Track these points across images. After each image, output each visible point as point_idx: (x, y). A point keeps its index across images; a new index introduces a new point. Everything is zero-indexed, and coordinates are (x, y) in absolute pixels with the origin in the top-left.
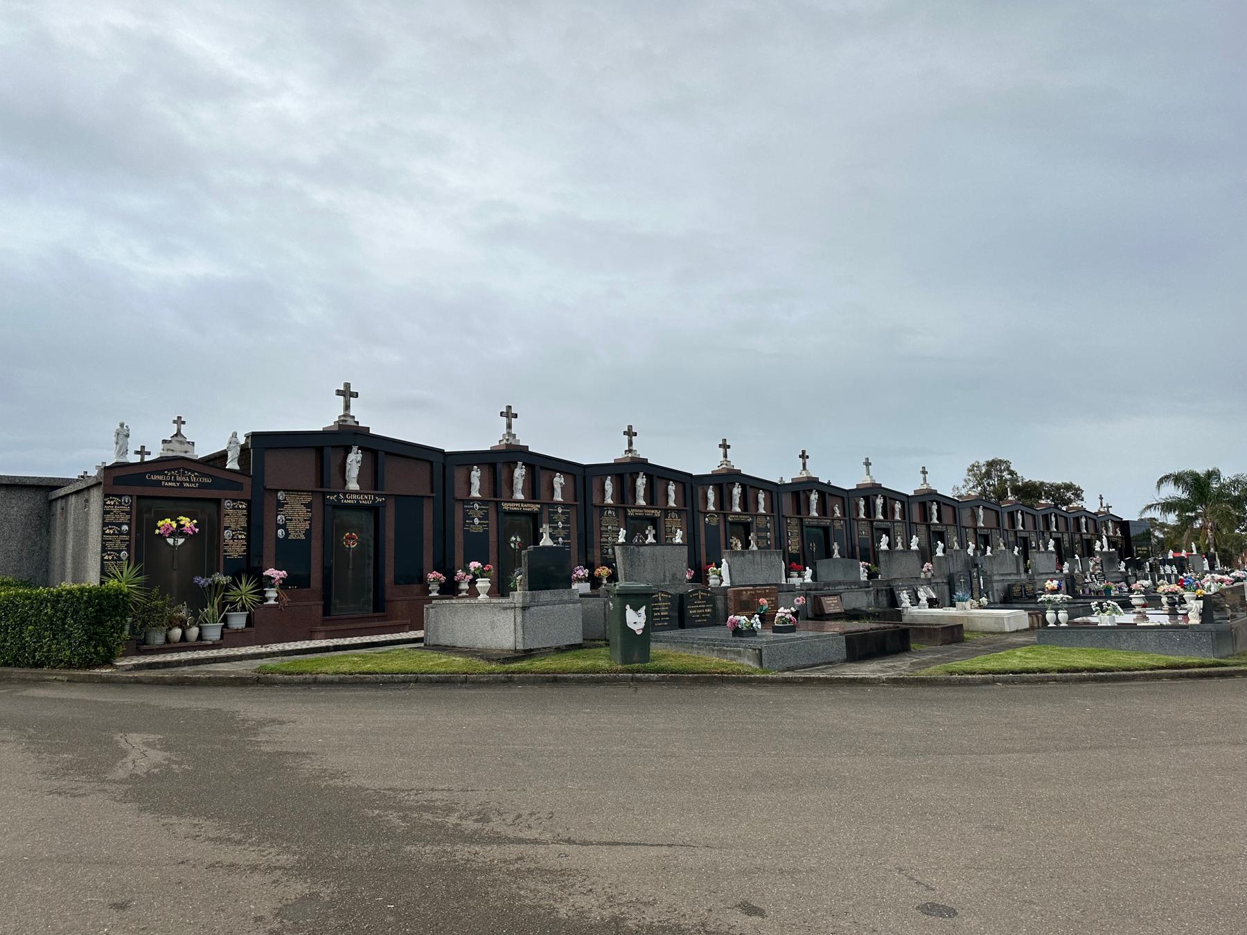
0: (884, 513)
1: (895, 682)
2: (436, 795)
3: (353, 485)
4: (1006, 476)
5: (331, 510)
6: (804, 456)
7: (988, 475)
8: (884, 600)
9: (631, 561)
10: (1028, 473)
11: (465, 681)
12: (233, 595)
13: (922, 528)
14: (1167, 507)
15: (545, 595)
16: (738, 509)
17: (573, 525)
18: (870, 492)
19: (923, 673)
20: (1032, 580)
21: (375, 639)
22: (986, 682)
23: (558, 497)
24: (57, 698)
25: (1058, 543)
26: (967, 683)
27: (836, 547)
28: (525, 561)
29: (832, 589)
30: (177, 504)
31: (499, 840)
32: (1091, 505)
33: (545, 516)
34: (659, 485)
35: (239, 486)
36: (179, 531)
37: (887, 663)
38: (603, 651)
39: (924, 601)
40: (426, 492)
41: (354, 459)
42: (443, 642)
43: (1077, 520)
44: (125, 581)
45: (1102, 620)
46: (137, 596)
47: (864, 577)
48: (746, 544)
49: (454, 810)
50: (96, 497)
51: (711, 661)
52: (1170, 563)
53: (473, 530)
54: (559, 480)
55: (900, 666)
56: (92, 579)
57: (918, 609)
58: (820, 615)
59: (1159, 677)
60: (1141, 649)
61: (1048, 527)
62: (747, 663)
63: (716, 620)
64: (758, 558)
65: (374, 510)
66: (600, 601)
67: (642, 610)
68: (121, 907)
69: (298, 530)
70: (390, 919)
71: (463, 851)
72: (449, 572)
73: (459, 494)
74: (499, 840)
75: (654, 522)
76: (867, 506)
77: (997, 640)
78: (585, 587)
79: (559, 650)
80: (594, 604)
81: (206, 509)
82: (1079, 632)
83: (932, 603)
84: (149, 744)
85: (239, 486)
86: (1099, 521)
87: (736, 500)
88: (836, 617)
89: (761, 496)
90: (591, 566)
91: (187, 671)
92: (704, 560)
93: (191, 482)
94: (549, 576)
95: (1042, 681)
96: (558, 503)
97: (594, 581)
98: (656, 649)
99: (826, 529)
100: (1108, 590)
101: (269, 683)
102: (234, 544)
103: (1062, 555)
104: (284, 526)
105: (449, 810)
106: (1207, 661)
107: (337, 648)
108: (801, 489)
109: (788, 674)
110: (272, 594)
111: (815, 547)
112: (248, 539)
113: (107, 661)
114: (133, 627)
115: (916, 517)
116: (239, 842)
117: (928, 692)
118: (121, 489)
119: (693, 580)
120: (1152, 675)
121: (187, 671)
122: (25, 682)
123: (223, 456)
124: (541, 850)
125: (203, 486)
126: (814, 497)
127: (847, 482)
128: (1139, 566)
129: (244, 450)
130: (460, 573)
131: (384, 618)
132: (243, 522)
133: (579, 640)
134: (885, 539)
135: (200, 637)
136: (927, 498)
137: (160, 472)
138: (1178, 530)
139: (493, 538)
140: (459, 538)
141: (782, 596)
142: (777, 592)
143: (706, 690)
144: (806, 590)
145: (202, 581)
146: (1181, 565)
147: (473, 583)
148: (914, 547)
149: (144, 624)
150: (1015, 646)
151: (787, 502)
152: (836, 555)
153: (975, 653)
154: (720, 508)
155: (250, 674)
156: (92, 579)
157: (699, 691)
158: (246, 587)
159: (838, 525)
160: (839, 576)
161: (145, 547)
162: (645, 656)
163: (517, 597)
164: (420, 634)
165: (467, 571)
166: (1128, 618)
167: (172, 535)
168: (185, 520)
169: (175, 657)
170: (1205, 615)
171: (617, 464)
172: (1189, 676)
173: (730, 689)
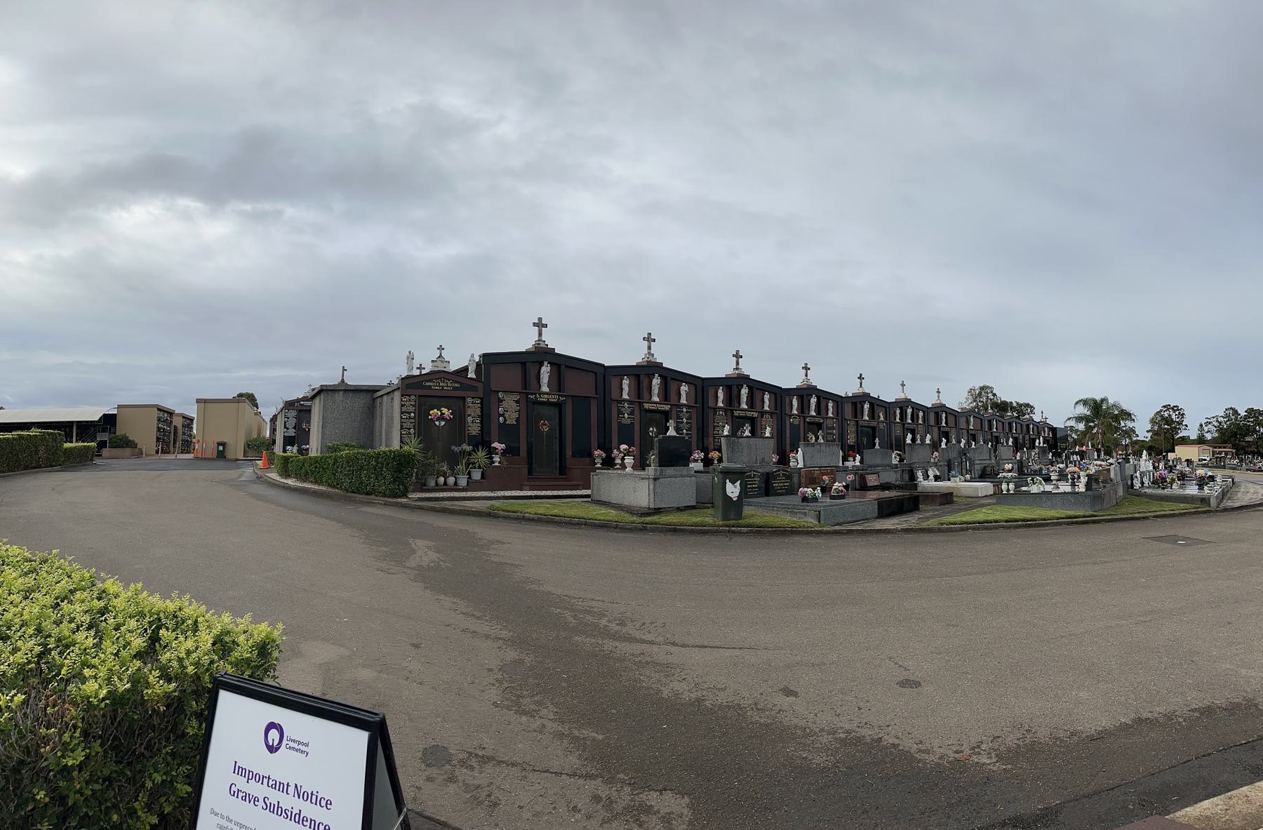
0: (912, 419)
1: (906, 531)
2: (594, 604)
3: (545, 389)
4: (990, 396)
5: (531, 405)
6: (861, 378)
7: (980, 394)
8: (906, 477)
9: (732, 447)
10: (1004, 395)
11: (616, 527)
12: (473, 458)
13: (936, 429)
14: (1079, 419)
15: (670, 471)
16: (813, 413)
17: (694, 421)
18: (903, 404)
19: (924, 525)
20: (998, 464)
21: (560, 493)
22: (962, 529)
23: (683, 401)
24: (379, 513)
25: (1016, 440)
26: (950, 530)
27: (877, 441)
28: (656, 445)
29: (873, 469)
30: (442, 399)
31: (630, 639)
32: (1037, 418)
33: (674, 414)
34: (757, 394)
35: (476, 389)
36: (442, 418)
37: (903, 518)
38: (710, 511)
39: (931, 477)
40: (592, 394)
41: (546, 370)
42: (604, 498)
43: (1028, 426)
44: (412, 447)
45: (1034, 489)
46: (419, 456)
47: (895, 461)
48: (817, 438)
49: (605, 616)
50: (397, 395)
51: (786, 519)
52: (1077, 453)
53: (624, 421)
54: (684, 388)
55: (911, 520)
56: (396, 445)
57: (927, 483)
58: (864, 487)
59: (1060, 524)
60: (1053, 507)
61: (1011, 430)
62: (810, 521)
63: (791, 491)
64: (823, 448)
65: (559, 406)
66: (709, 476)
67: (738, 484)
68: (416, 646)
69: (511, 418)
70: (564, 684)
71: (609, 645)
72: (609, 451)
73: (615, 396)
74: (630, 639)
75: (752, 421)
76: (901, 414)
77: (974, 502)
78: (699, 466)
79: (679, 509)
80: (705, 478)
81: (456, 403)
82: (1020, 497)
83: (937, 478)
84: (429, 548)
85: (476, 389)
86: (1040, 427)
87: (813, 407)
88: (875, 488)
89: (830, 405)
90: (706, 451)
91: (447, 504)
92: (788, 449)
93: (448, 385)
94: (674, 456)
95: (996, 528)
96: (684, 405)
97: (707, 462)
98: (747, 510)
99: (874, 429)
100: (1041, 470)
101: (496, 517)
102: (474, 428)
103: (1017, 447)
104: (503, 415)
105: (602, 615)
106: (1087, 513)
107: (537, 497)
108: (857, 401)
109: (837, 528)
110: (497, 459)
111: (865, 441)
112: (482, 423)
113: (404, 495)
114: (417, 477)
115: (932, 422)
116: (479, 618)
117: (926, 537)
118: (409, 391)
119: (778, 463)
120: (1057, 523)
121: (447, 504)
122: (362, 503)
123: (466, 369)
124: (656, 648)
125: (455, 389)
126: (867, 406)
127: (889, 397)
128: (1060, 455)
129: (478, 365)
130: (615, 451)
131: (566, 480)
132: (478, 412)
133: (693, 503)
134: (909, 436)
135: (456, 484)
136: (939, 409)
137: (430, 381)
138: (1084, 434)
139: (637, 428)
140: (615, 427)
141: (839, 475)
142: (834, 472)
143: (780, 539)
144: (855, 470)
145: (456, 449)
146: (1082, 455)
147: (623, 459)
148: (928, 442)
149: (424, 473)
150: (983, 506)
151: (848, 409)
152: (877, 447)
153: (959, 511)
154: (798, 414)
155: (485, 510)
156: (396, 445)
157: (775, 541)
158: (481, 454)
159: (881, 426)
160: (878, 461)
161: (423, 426)
162: (739, 515)
163: (651, 471)
164: (588, 492)
165: (619, 449)
166: (1049, 488)
167: (438, 419)
168: (445, 410)
169: (441, 495)
170: (1088, 486)
171: (727, 378)
172: (1077, 523)
173: (797, 538)
